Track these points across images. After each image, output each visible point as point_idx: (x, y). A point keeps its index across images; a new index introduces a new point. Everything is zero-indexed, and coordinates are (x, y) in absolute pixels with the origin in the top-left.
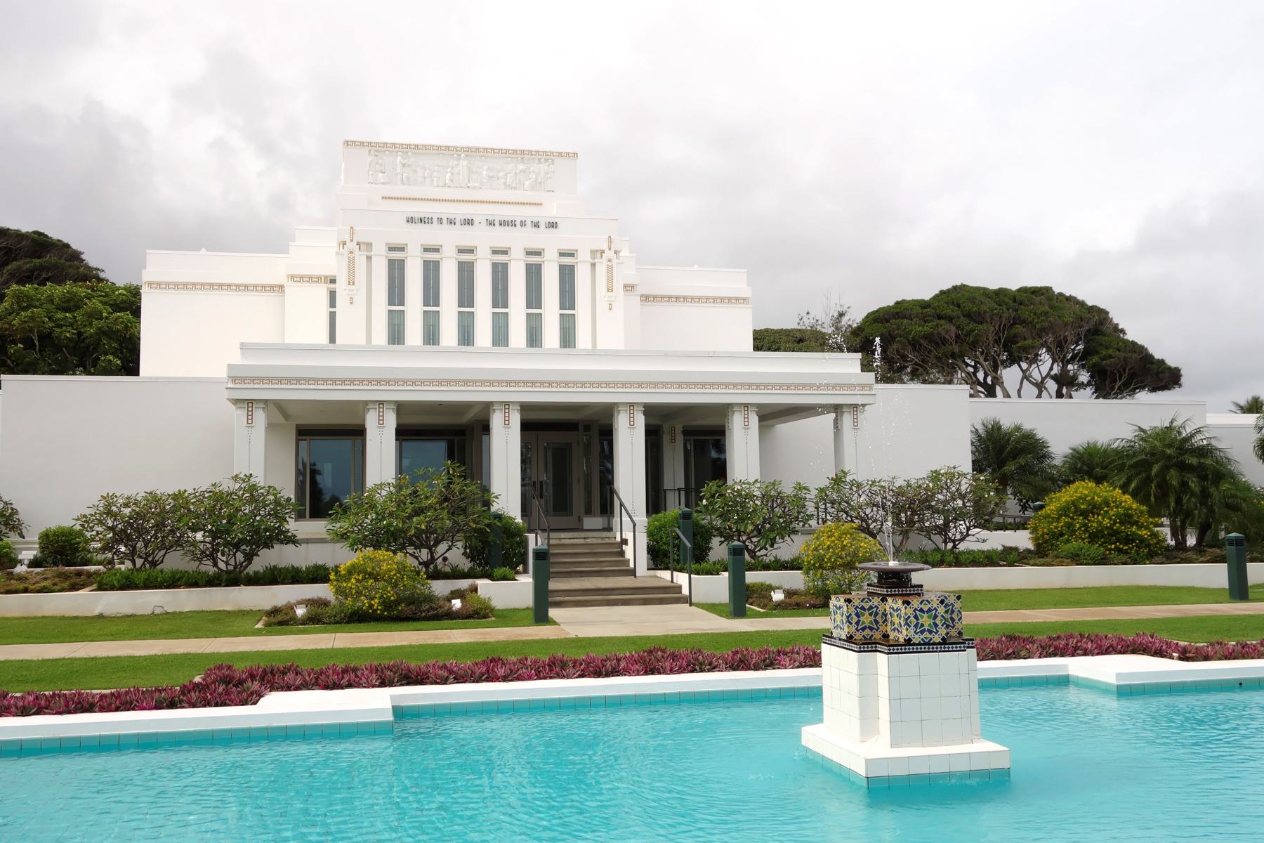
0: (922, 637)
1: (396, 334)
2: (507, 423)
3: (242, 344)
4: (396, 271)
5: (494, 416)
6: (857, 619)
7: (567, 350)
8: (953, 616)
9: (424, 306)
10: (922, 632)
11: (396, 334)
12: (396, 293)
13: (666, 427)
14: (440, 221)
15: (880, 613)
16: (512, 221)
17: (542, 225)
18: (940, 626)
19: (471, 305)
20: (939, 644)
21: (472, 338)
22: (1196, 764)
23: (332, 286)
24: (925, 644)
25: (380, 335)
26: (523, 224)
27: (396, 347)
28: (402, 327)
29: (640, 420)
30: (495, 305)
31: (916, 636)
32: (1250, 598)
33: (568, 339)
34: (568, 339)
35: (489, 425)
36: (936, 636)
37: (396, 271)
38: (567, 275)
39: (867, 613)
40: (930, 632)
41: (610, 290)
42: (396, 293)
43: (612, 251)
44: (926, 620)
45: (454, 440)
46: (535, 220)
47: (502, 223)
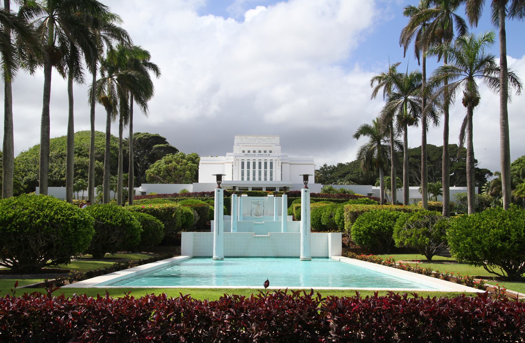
1: (243, 179)
11: (243, 179)
25: (240, 179)
33: (271, 179)
34: (271, 179)
37: (243, 163)
38: (271, 164)
41: (279, 166)
42: (243, 167)
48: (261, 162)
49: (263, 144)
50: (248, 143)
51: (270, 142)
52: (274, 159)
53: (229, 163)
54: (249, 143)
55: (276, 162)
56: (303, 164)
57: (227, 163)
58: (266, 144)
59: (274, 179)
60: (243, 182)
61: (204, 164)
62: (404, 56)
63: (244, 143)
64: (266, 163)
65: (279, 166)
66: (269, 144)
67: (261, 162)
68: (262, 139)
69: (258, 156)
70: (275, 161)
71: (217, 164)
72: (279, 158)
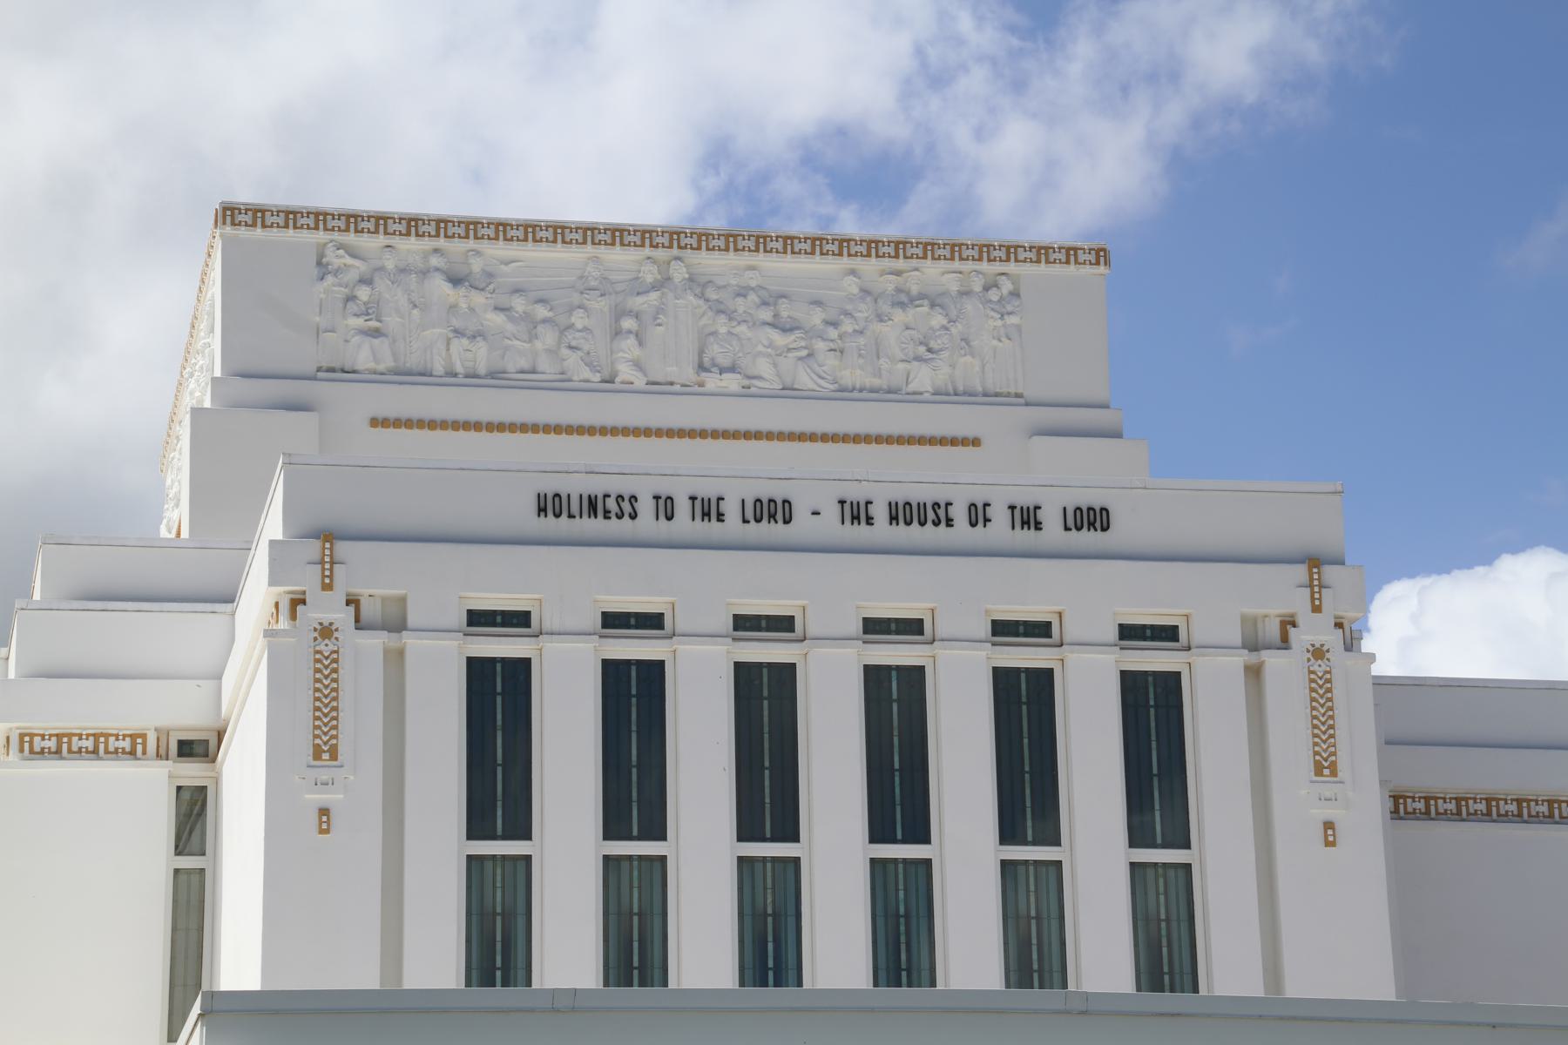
7: (1034, 997)
14: (665, 507)
16: (936, 505)
17: (1051, 518)
19: (919, 832)
21: (521, 962)
23: (191, 773)
26: (978, 515)
28: (521, 921)
30: (879, 832)
41: (1325, 766)
43: (339, 596)
46: (1025, 499)
47: (901, 513)
49: (789, 391)
50: (496, 377)
51: (928, 351)
53: (98, 747)
54: (528, 379)
55: (1254, 673)
56: (1492, 810)
58: (845, 393)
62: (976, 442)
63: (405, 374)
65: (1325, 766)
66: (915, 397)
68: (770, 299)
69: (831, 526)
72: (1316, 587)
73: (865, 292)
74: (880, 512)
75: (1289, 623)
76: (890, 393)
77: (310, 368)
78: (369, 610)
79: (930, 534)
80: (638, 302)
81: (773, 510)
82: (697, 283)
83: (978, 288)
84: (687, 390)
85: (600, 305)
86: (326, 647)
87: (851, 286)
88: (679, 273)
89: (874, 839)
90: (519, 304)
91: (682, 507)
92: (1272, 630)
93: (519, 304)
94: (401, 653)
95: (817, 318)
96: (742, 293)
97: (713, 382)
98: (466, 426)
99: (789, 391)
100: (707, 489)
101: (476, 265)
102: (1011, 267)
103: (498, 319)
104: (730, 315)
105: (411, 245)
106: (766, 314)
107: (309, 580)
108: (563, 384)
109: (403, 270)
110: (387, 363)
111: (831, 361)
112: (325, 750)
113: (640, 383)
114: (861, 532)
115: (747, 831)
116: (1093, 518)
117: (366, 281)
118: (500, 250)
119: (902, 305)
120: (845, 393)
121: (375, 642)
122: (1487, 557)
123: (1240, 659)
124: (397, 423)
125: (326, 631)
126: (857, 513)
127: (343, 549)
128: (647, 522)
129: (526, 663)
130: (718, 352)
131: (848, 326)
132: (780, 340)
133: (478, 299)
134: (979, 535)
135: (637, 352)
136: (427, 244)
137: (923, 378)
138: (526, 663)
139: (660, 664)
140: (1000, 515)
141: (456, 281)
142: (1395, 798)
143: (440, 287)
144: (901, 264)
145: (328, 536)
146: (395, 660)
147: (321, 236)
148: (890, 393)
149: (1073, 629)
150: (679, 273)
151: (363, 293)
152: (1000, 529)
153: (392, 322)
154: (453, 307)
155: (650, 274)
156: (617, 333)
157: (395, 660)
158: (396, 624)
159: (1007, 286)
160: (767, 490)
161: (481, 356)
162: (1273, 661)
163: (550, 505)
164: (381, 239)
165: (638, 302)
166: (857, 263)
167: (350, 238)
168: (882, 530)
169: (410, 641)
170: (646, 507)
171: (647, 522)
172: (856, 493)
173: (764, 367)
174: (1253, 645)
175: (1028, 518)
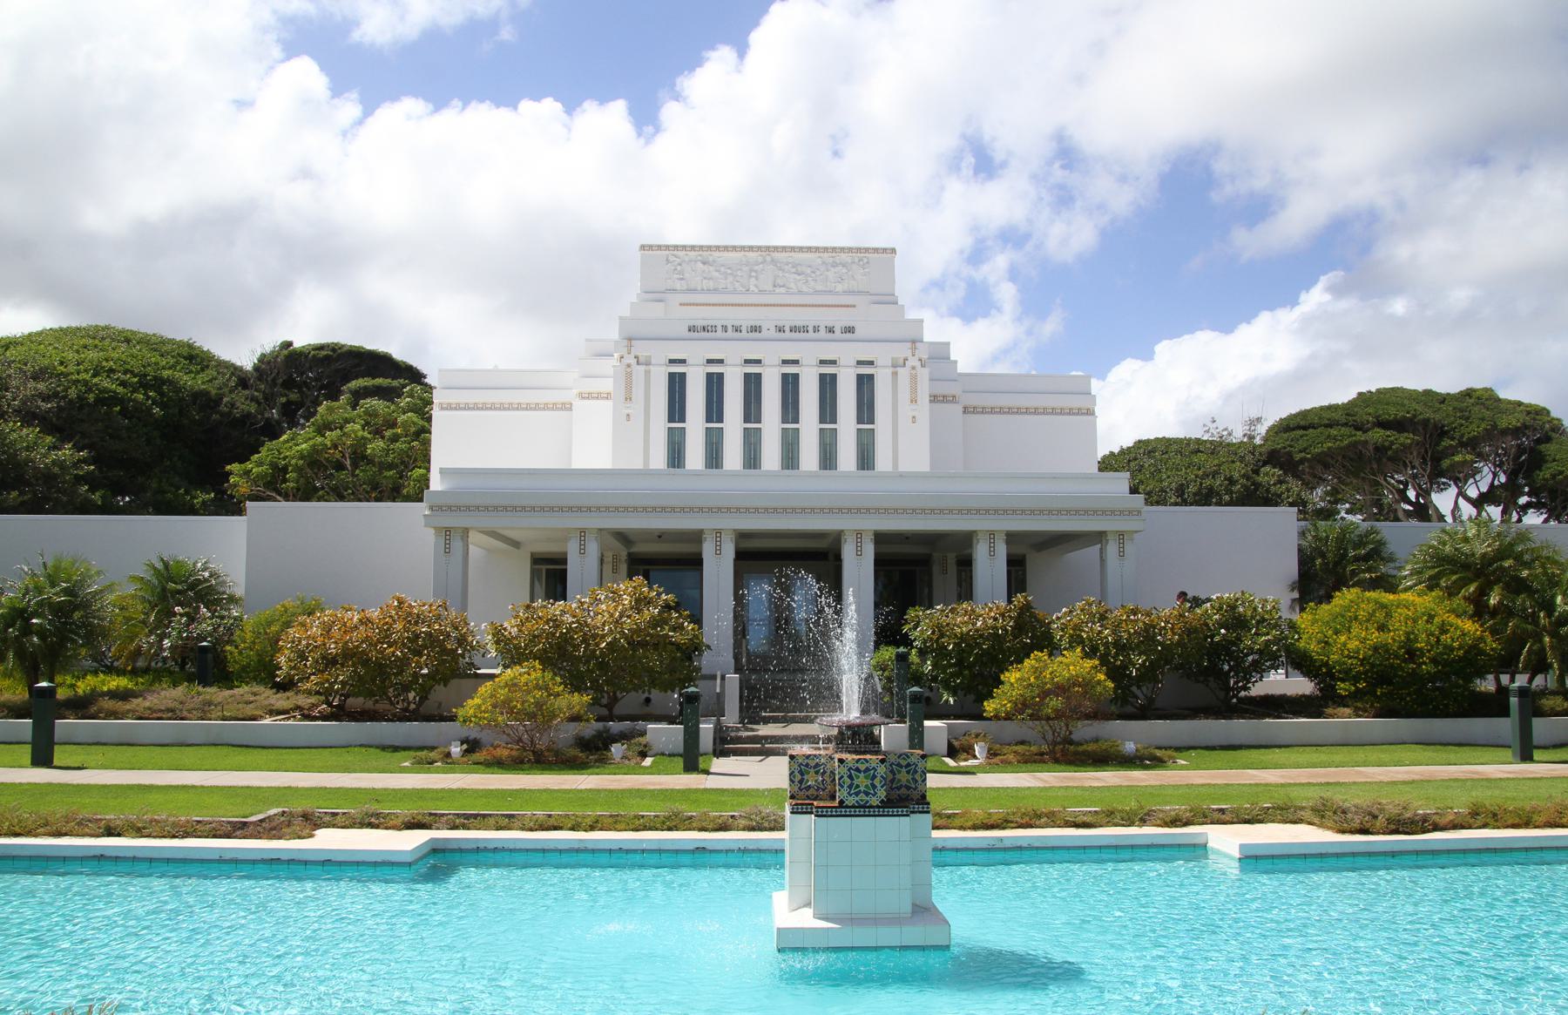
0: (857, 799)
1: (676, 456)
2: (718, 552)
3: (441, 469)
4: (677, 385)
5: (979, 547)
6: (800, 777)
8: (800, 777)
9: (783, 423)
10: (857, 794)
11: (676, 456)
12: (676, 410)
13: (936, 555)
14: (725, 329)
15: (829, 771)
17: (837, 330)
18: (879, 788)
20: (878, 807)
22: (891, 961)
24: (860, 807)
25: (659, 460)
26: (816, 329)
27: (715, 471)
29: (1002, 550)
31: (878, 795)
32: (56, 762)
33: (866, 459)
34: (866, 459)
35: (840, 555)
36: (874, 799)
37: (677, 385)
38: (865, 384)
39: (812, 771)
40: (867, 794)
41: (913, 401)
42: (676, 410)
43: (632, 355)
44: (862, 781)
45: (541, 570)
46: (830, 324)
48: (683, 376)
49: (800, 292)
52: (882, 355)
54: (724, 291)
55: (895, 374)
57: (588, 396)
58: (817, 292)
59: (883, 461)
60: (676, 484)
61: (458, 407)
62: (854, 306)
64: (715, 385)
66: (837, 293)
67: (683, 376)
69: (773, 333)
70: (889, 371)
71: (536, 407)
72: (914, 349)
73: (824, 263)
74: (787, 329)
75: (906, 359)
76: (830, 292)
77: (663, 289)
78: (641, 360)
79: (802, 335)
80: (756, 268)
81: (755, 329)
82: (773, 261)
83: (856, 260)
84: (771, 293)
85: (746, 269)
86: (629, 370)
87: (819, 261)
88: (768, 259)
89: (745, 422)
90: (722, 269)
91: (730, 329)
92: (901, 362)
93: (722, 269)
94: (649, 372)
95: (808, 271)
96: (787, 264)
97: (778, 290)
98: (707, 305)
99: (800, 292)
100: (737, 324)
101: (711, 259)
102: (867, 255)
103: (717, 274)
104: (783, 271)
105: (693, 253)
106: (794, 270)
107: (624, 351)
108: (735, 292)
109: (691, 261)
110: (685, 288)
111: (812, 283)
112: (628, 399)
113: (756, 291)
114: (781, 335)
115: (822, 421)
116: (850, 330)
117: (680, 265)
118: (717, 254)
119: (833, 266)
120: (817, 292)
121: (642, 368)
122: (1179, 336)
123: (891, 370)
124: (687, 305)
125: (629, 366)
126: (781, 330)
127: (633, 342)
128: (720, 333)
129: (685, 374)
130: (779, 281)
131: (818, 273)
132: (798, 278)
133: (711, 268)
134: (816, 335)
135: (755, 282)
136: (697, 253)
137: (840, 288)
138: (685, 374)
139: (723, 374)
140: (822, 329)
141: (704, 263)
142: (965, 408)
143: (700, 265)
144: (834, 254)
145: (630, 339)
146: (648, 373)
147: (667, 252)
148: (830, 292)
149: (842, 362)
150: (768, 259)
151: (679, 268)
152: (823, 333)
153: (687, 275)
154: (704, 271)
155: (760, 259)
156: (750, 276)
157: (648, 373)
158: (648, 364)
159: (865, 260)
160: (754, 324)
161: (711, 285)
162: (900, 370)
163: (692, 329)
164: (684, 252)
165: (756, 268)
166: (822, 254)
167: (675, 252)
168: (788, 334)
169: (651, 367)
170: (719, 328)
171: (720, 333)
172: (780, 324)
173: (792, 285)
174: (894, 366)
175: (831, 330)
